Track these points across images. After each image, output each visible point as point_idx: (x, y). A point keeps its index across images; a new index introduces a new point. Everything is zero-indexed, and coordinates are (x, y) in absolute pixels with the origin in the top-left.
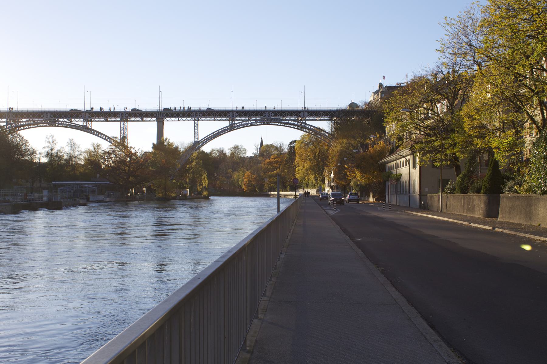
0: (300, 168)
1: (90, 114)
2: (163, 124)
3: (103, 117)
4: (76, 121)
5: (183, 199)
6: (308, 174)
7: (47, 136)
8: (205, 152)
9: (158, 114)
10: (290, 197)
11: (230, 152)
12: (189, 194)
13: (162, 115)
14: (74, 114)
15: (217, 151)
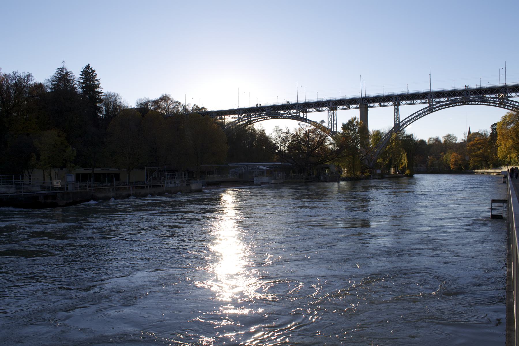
0: (502, 146)
2: (368, 110)
6: (510, 153)
8: (426, 140)
10: (492, 174)
11: (444, 140)
12: (106, 179)
14: (289, 107)
15: (434, 139)
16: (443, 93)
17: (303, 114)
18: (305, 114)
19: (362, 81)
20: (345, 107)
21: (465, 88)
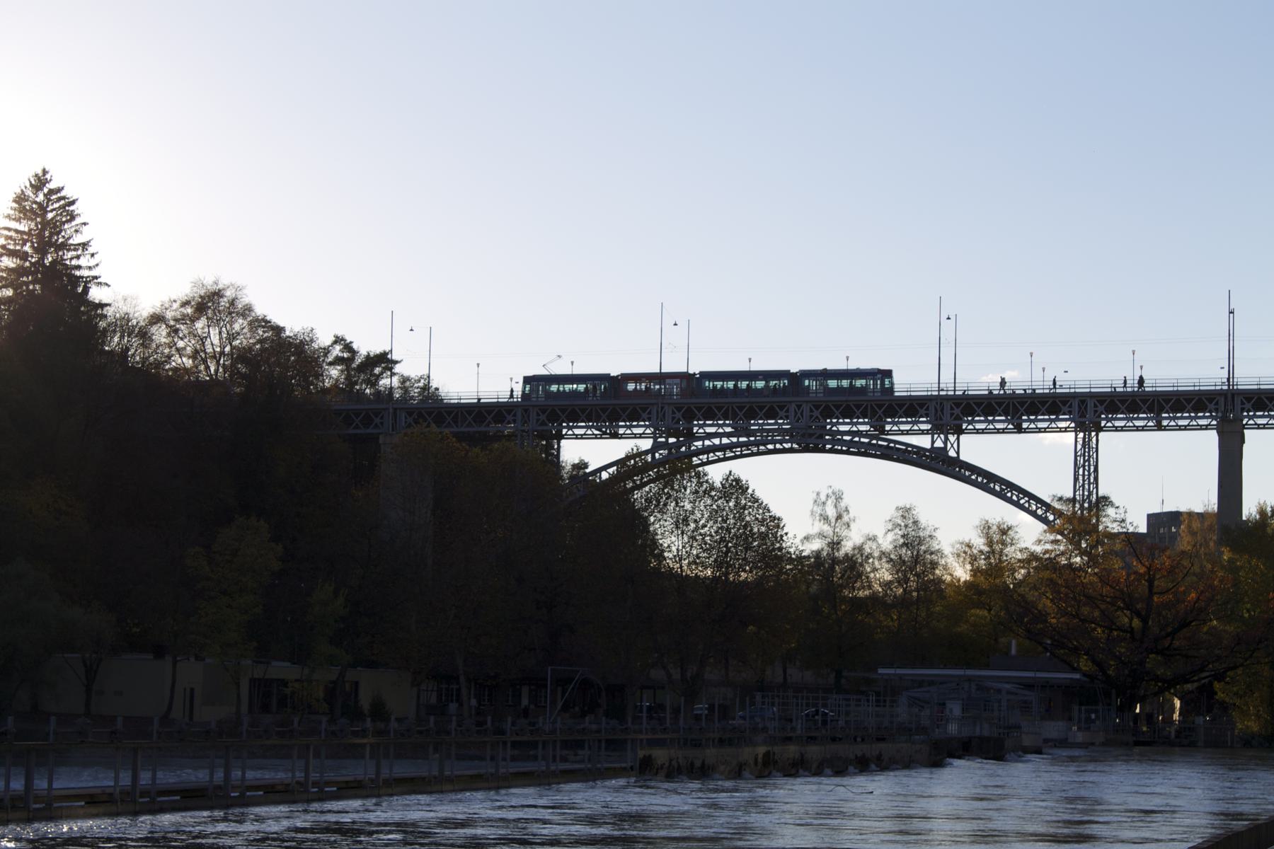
1: (679, 409)
2: (1242, 440)
4: (903, 433)
7: (818, 494)
13: (1238, 407)
16: (968, 404)
19: (944, 317)
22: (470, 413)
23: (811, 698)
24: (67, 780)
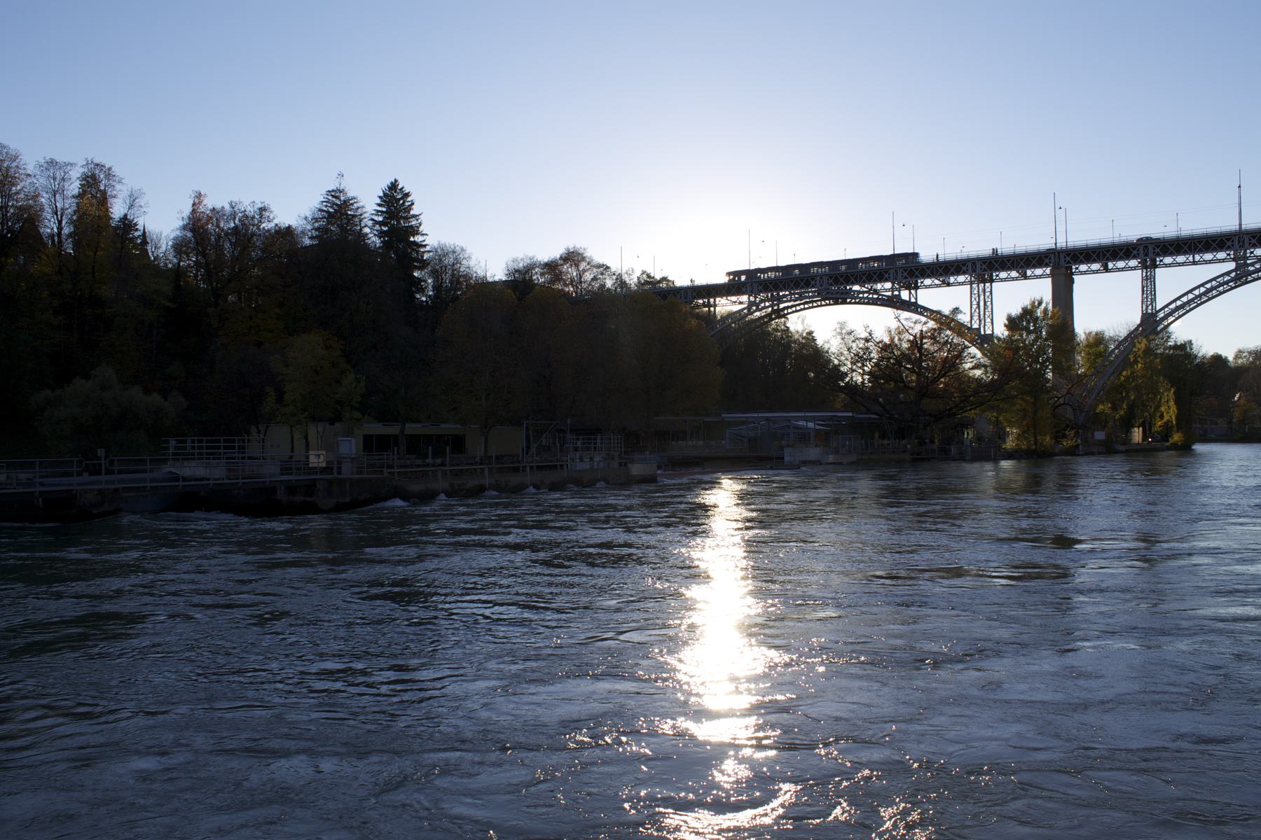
2: (1072, 281)
3: (1014, 267)
5: (1099, 453)
9: (1053, 258)
15: (1250, 353)
17: (908, 291)
18: (913, 292)
19: (1057, 207)
20: (1014, 274)
21: (1238, 227)
22: (724, 288)
23: (396, 474)
24: (111, 622)
